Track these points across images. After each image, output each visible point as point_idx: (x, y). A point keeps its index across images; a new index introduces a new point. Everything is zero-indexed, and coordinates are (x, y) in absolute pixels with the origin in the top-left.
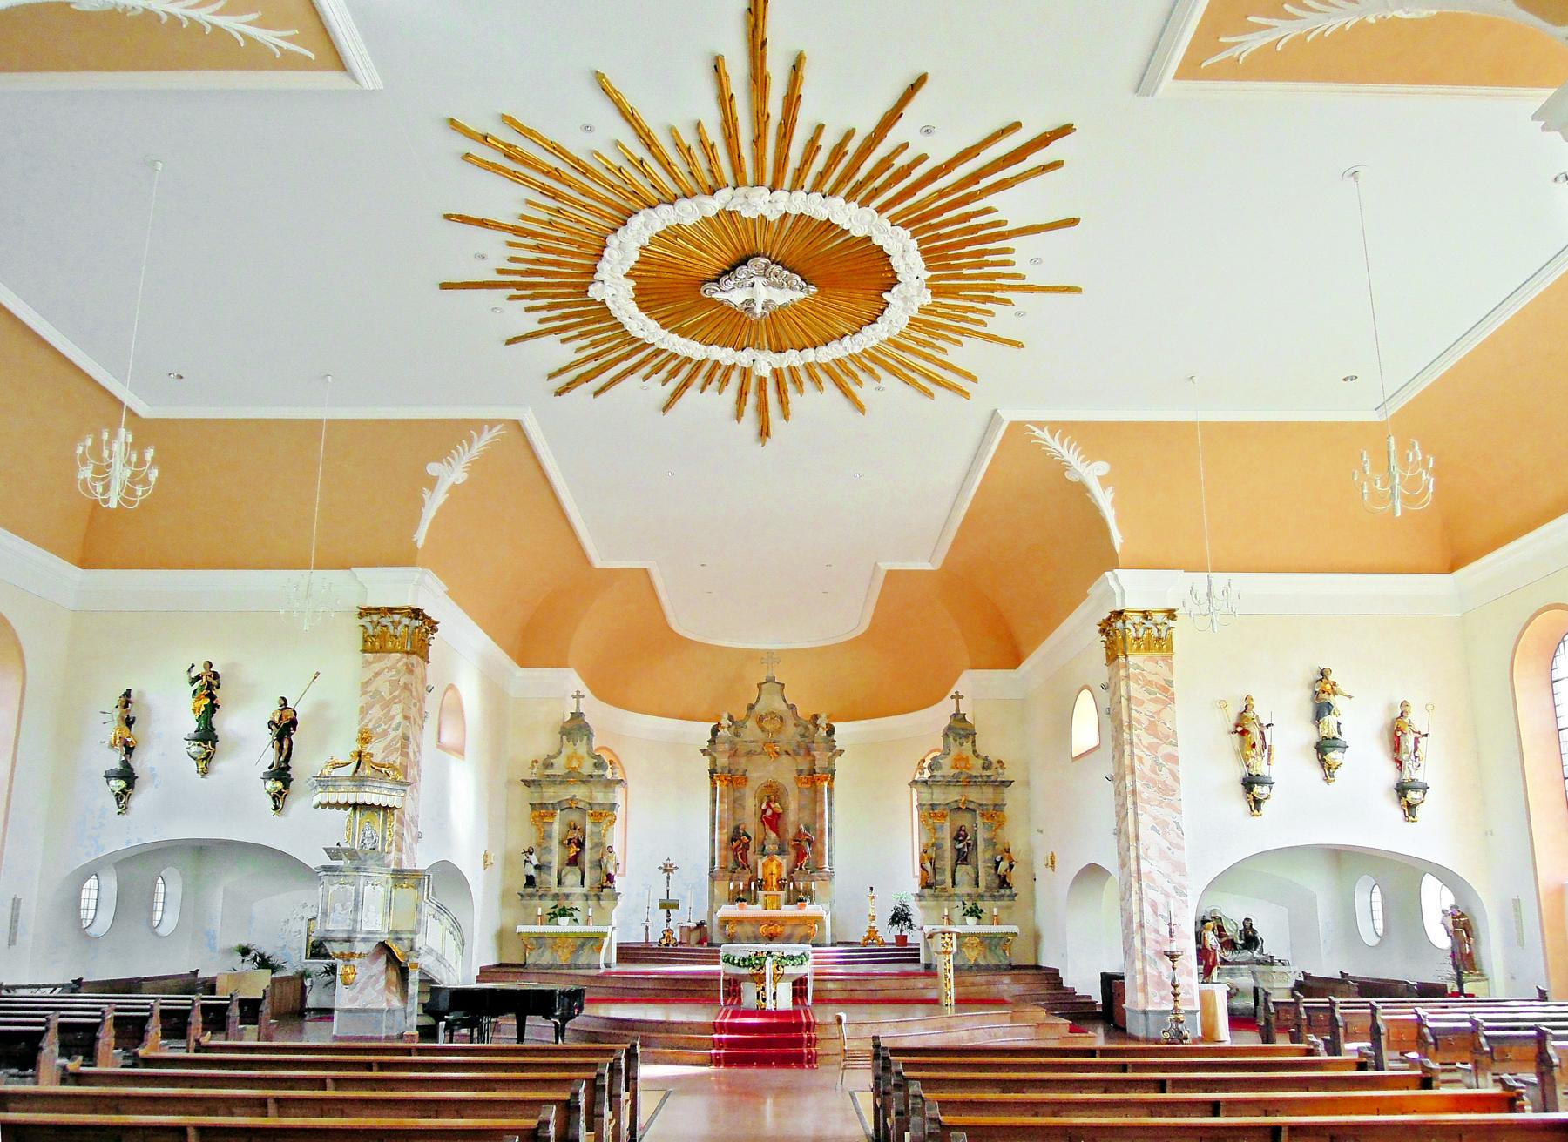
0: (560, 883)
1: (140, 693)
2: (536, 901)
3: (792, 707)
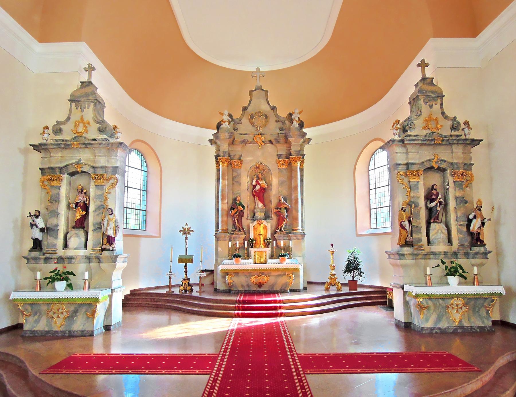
0: (66, 246)
2: (42, 265)
3: (273, 108)
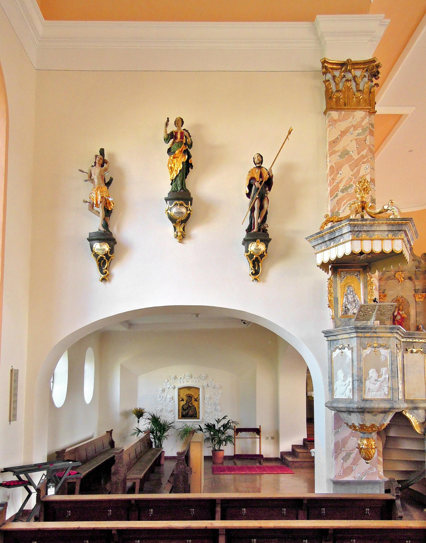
1: (112, 156)
